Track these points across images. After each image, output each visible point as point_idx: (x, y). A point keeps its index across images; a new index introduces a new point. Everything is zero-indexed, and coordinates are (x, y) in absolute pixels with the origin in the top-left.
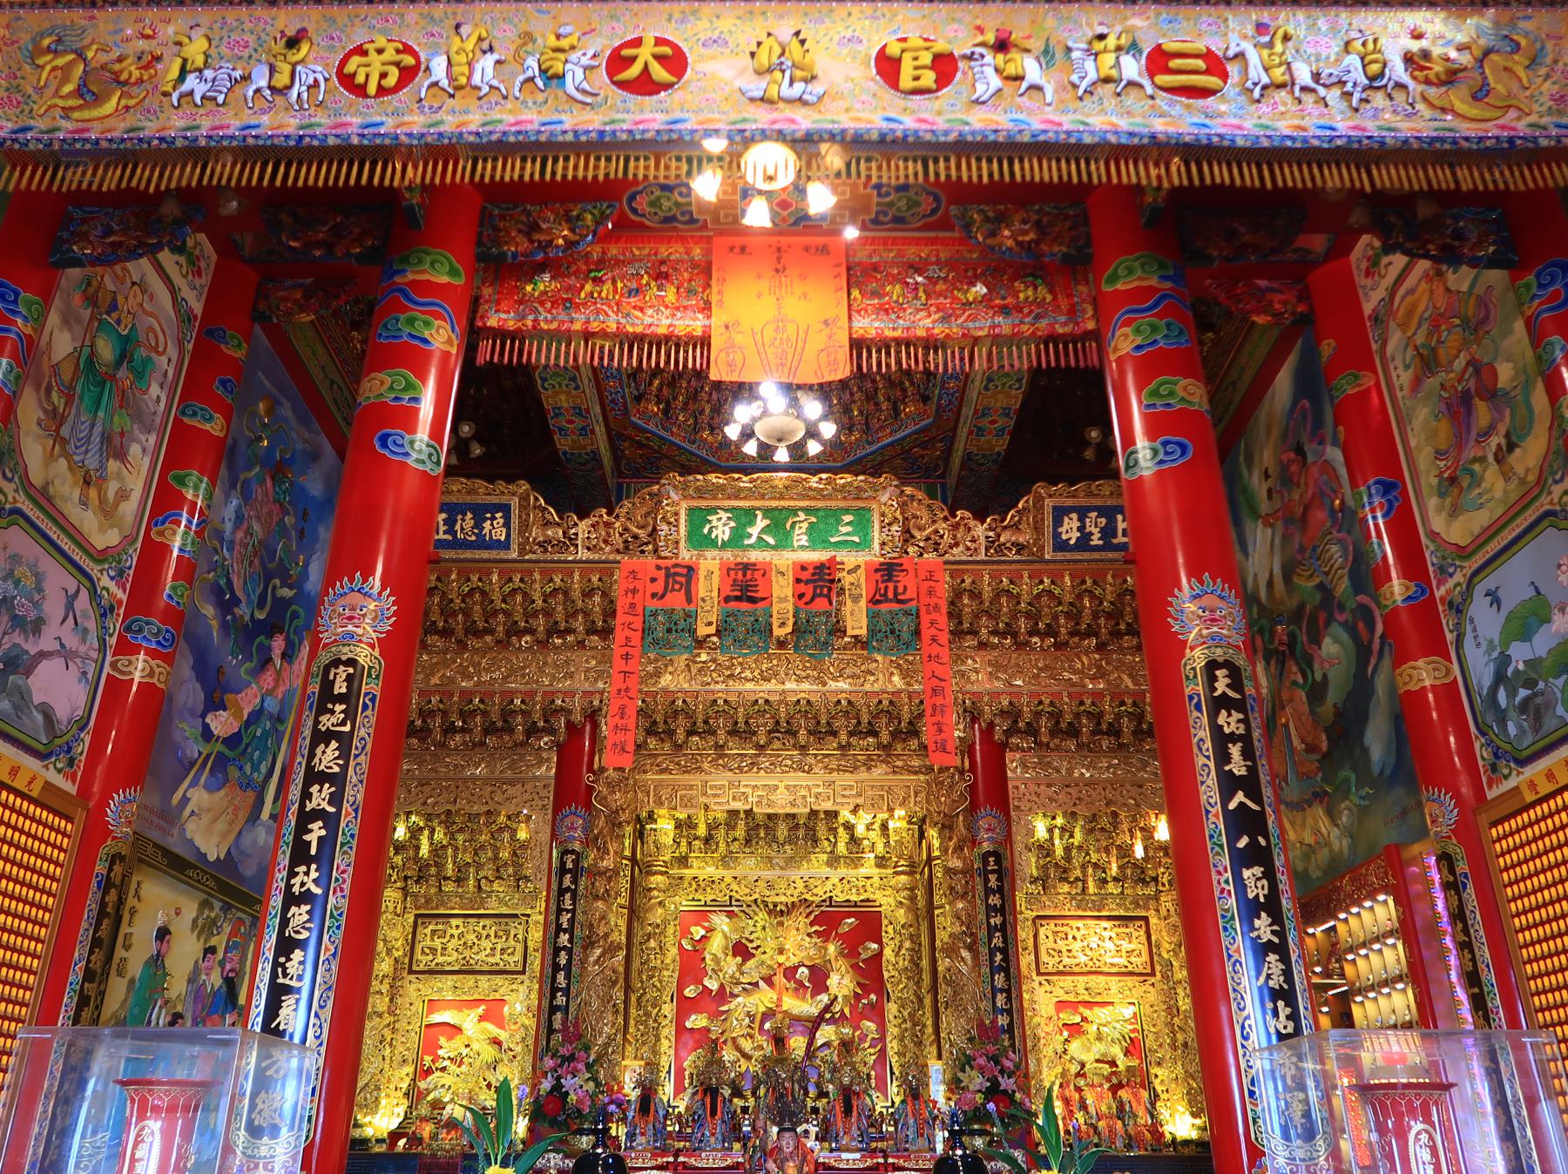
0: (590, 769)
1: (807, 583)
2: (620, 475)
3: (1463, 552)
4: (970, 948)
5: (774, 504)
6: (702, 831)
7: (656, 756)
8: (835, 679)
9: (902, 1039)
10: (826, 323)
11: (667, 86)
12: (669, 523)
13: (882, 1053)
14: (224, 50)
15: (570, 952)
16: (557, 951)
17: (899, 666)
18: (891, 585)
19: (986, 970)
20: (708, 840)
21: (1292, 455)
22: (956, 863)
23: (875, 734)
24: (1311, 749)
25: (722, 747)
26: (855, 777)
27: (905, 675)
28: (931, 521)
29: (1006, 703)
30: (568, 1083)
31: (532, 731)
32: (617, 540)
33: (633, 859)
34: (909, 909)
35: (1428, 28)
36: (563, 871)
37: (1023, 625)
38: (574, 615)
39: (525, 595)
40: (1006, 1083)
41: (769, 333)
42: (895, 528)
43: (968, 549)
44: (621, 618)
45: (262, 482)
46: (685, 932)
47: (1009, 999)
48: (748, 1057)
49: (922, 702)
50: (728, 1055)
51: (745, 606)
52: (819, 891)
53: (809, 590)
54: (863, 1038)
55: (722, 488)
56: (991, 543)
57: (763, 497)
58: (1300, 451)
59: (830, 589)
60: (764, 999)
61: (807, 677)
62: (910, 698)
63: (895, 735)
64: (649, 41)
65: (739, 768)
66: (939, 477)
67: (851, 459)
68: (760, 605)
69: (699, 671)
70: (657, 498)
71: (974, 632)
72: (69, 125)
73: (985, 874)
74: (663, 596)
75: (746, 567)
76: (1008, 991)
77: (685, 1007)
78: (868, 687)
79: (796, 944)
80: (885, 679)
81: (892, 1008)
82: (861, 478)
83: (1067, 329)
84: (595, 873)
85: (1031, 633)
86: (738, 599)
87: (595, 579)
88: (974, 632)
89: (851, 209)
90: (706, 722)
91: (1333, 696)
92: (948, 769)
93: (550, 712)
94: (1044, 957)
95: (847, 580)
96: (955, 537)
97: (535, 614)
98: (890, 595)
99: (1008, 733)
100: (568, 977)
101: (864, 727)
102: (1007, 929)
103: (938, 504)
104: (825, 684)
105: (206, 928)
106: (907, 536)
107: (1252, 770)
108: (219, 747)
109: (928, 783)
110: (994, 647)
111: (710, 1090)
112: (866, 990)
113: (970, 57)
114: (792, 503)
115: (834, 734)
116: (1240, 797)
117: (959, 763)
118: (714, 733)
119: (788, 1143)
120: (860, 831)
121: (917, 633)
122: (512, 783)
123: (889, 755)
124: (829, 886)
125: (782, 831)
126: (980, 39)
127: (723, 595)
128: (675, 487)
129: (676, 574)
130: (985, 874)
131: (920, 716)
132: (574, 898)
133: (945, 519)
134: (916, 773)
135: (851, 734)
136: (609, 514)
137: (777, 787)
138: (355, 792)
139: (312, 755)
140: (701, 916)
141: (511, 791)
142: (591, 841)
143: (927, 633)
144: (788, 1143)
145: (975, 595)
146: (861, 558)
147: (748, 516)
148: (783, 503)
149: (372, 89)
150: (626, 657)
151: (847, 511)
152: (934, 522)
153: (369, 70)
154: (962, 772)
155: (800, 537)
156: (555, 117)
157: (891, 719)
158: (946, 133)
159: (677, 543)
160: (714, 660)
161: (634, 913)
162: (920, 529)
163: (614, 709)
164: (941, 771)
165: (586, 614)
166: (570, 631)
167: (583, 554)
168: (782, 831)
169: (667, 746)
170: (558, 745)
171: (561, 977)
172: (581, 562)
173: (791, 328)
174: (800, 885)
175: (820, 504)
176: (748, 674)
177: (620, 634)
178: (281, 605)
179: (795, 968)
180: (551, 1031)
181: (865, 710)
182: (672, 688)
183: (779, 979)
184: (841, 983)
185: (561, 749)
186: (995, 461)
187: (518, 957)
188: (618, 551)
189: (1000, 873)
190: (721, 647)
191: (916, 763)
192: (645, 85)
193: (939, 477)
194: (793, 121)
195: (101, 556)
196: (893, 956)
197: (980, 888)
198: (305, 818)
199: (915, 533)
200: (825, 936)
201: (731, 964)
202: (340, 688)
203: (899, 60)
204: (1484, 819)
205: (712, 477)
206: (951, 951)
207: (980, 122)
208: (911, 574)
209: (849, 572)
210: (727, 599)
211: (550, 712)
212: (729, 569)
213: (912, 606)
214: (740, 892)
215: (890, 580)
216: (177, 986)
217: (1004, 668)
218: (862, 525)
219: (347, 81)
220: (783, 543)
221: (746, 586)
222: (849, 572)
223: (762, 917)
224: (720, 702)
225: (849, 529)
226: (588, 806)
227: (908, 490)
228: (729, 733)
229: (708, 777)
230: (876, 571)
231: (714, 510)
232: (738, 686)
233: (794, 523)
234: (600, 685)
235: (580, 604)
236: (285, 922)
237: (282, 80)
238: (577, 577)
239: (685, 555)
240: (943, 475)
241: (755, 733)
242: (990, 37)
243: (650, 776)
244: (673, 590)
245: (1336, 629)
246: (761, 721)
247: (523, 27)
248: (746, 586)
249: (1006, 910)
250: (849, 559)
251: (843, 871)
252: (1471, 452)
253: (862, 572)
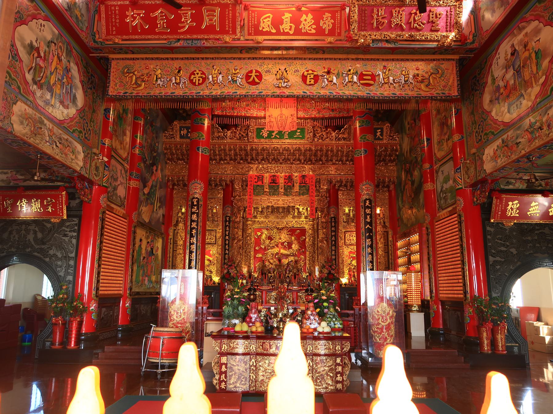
3: (440, 160)
4: (326, 241)
6: (260, 210)
9: (309, 261)
10: (292, 115)
11: (258, 83)
13: (305, 264)
14: (164, 73)
15: (229, 240)
16: (226, 240)
17: (312, 169)
19: (330, 245)
20: (261, 212)
21: (413, 121)
22: (324, 220)
24: (411, 196)
30: (230, 271)
31: (216, 185)
33: (243, 217)
34: (312, 230)
35: (420, 67)
36: (226, 221)
37: (344, 158)
39: (214, 151)
40: (332, 272)
41: (279, 118)
42: (311, 134)
45: (149, 129)
46: (256, 234)
47: (335, 252)
48: (272, 264)
50: (267, 263)
51: (274, 184)
52: (290, 224)
54: (300, 260)
58: (415, 121)
60: (276, 250)
64: (254, 71)
71: (331, 160)
72: (135, 92)
73: (331, 222)
76: (335, 251)
77: (256, 252)
79: (284, 237)
81: (308, 253)
83: (347, 115)
84: (234, 222)
85: (346, 161)
88: (331, 160)
91: (416, 185)
93: (221, 180)
94: (347, 241)
97: (216, 155)
99: (339, 187)
100: (228, 246)
102: (336, 236)
105: (147, 238)
106: (315, 135)
107: (371, 221)
108: (146, 196)
110: (337, 164)
111: (263, 272)
112: (302, 248)
113: (322, 76)
116: (368, 226)
119: (282, 286)
120: (301, 210)
122: (212, 199)
124: (292, 223)
125: (281, 210)
126: (324, 71)
130: (331, 222)
132: (229, 228)
138: (200, 224)
139: (191, 217)
140: (260, 230)
141: (212, 200)
142: (233, 214)
144: (282, 286)
149: (197, 84)
150: (250, 195)
153: (196, 78)
154: (326, 197)
156: (236, 91)
158: (316, 96)
160: (263, 167)
161: (244, 231)
166: (225, 160)
167: (229, 141)
168: (281, 210)
171: (227, 246)
173: (284, 117)
174: (285, 223)
178: (154, 157)
179: (284, 243)
180: (225, 259)
183: (280, 245)
184: (295, 247)
185: (224, 190)
187: (214, 240)
189: (335, 222)
192: (254, 83)
194: (284, 93)
195: (124, 160)
196: (308, 241)
197: (330, 226)
198: (192, 229)
200: (292, 235)
201: (267, 242)
202: (195, 203)
203: (307, 76)
204: (435, 221)
206: (322, 241)
207: (322, 92)
211: (221, 180)
214: (270, 225)
216: (144, 251)
217: (339, 170)
219: (191, 81)
223: (275, 230)
226: (232, 205)
236: (190, 248)
237: (178, 81)
242: (326, 70)
245: (417, 169)
247: (227, 67)
248: (274, 180)
249: (336, 231)
251: (296, 219)
252: (443, 137)
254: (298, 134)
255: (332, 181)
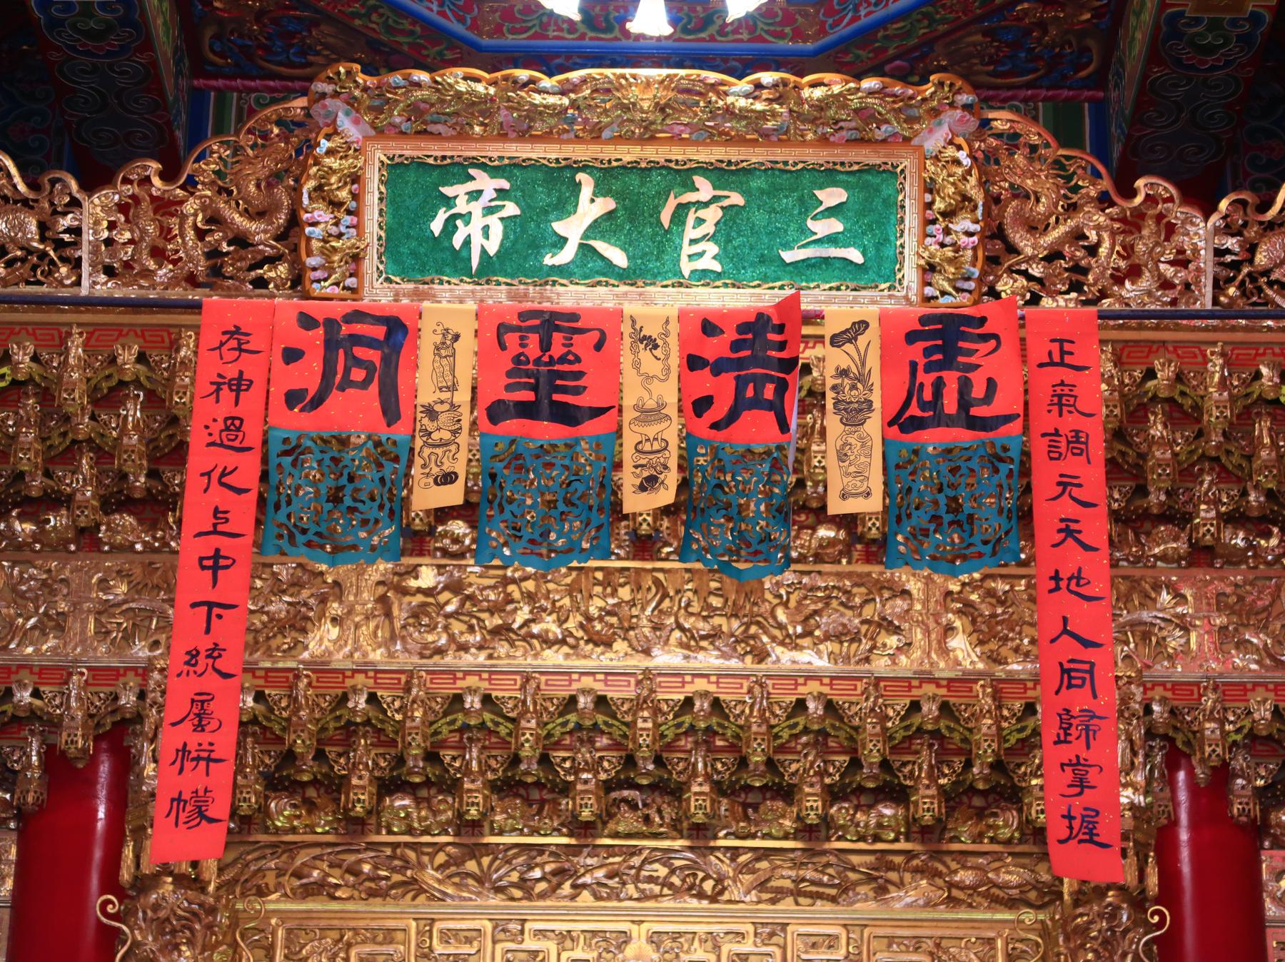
0: (110, 882)
1: (718, 368)
2: (200, 68)
5: (628, 153)
7: (293, 848)
8: (790, 642)
12: (335, 205)
17: (968, 610)
18: (951, 379)
23: (898, 794)
25: (476, 826)
26: (842, 912)
27: (984, 632)
28: (1069, 212)
29: (1263, 713)
32: (189, 247)
38: (68, 456)
42: (963, 223)
43: (1166, 284)
44: (200, 457)
49: (1030, 709)
51: (546, 432)
53: (723, 389)
55: (482, 108)
56: (1228, 268)
57: (595, 134)
59: (782, 387)
61: (714, 636)
62: (997, 696)
63: (955, 798)
65: (523, 884)
66: (1086, 84)
67: (843, 30)
68: (590, 428)
69: (416, 614)
70: (302, 134)
71: (1178, 517)
74: (317, 402)
75: (552, 323)
78: (881, 665)
80: (930, 640)
82: (870, 83)
86: (526, 411)
87: (127, 357)
88: (1178, 517)
89: (93, 496)
90: (432, 757)
92: (1101, 892)
95: (827, 362)
96: (1128, 251)
98: (950, 404)
101: (868, 776)
103: (1083, 158)
104: (761, 656)
106: (997, 247)
109: (1044, 932)
110: (1234, 558)
114: (677, 153)
115: (787, 793)
117: (1130, 878)
118: (452, 787)
121: (1025, 516)
123: (937, 855)
127: (486, 400)
128: (352, 102)
129: (356, 340)
131: (1027, 746)
133: (1104, 201)
134: (1011, 904)
135: (833, 794)
136: (167, 176)
137: (625, 938)
143: (1048, 514)
145: (1184, 413)
146: (868, 305)
147: (558, 185)
148: (653, 153)
150: (215, 564)
151: (829, 176)
152: (1072, 208)
154: (1139, 902)
155: (698, 249)
157: (943, 755)
159: (357, 258)
162: (1035, 227)
163: (178, 705)
164: (1080, 899)
165: (103, 454)
166: (56, 500)
167: (94, 284)
169: (323, 824)
170: (21, 815)
172: (91, 303)
175: (756, 156)
176: (549, 625)
177: (197, 505)
181: (871, 726)
182: (339, 660)
186: (1245, 39)
188: (192, 280)
190: (481, 551)
191: (1011, 876)
193: (1086, 84)
199: (1025, 244)
205: (456, 78)
208: (1008, 350)
209: (836, 341)
210: (496, 412)
212: (502, 329)
213: (1010, 435)
215: (947, 364)
218: (871, 214)
220: (654, 260)
221: (548, 374)
222: (836, 341)
224: (472, 702)
225: (835, 226)
227: (1002, 120)
228: (494, 787)
229: (434, 909)
230: (912, 337)
231: (459, 171)
232: (522, 659)
233: (682, 209)
234: (140, 650)
235: (84, 425)
238: (76, 350)
239: (379, 293)
240: (1099, 80)
241: (566, 789)
243: (274, 902)
244: (347, 383)
246: (584, 755)
248: (548, 374)
250: (836, 306)
253: (870, 339)
254: (821, 228)
255: (1196, 737)
